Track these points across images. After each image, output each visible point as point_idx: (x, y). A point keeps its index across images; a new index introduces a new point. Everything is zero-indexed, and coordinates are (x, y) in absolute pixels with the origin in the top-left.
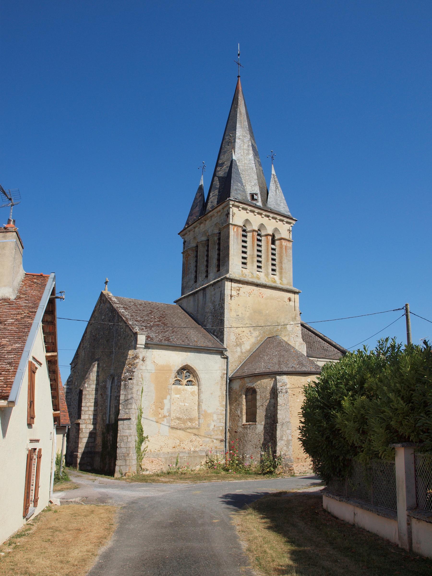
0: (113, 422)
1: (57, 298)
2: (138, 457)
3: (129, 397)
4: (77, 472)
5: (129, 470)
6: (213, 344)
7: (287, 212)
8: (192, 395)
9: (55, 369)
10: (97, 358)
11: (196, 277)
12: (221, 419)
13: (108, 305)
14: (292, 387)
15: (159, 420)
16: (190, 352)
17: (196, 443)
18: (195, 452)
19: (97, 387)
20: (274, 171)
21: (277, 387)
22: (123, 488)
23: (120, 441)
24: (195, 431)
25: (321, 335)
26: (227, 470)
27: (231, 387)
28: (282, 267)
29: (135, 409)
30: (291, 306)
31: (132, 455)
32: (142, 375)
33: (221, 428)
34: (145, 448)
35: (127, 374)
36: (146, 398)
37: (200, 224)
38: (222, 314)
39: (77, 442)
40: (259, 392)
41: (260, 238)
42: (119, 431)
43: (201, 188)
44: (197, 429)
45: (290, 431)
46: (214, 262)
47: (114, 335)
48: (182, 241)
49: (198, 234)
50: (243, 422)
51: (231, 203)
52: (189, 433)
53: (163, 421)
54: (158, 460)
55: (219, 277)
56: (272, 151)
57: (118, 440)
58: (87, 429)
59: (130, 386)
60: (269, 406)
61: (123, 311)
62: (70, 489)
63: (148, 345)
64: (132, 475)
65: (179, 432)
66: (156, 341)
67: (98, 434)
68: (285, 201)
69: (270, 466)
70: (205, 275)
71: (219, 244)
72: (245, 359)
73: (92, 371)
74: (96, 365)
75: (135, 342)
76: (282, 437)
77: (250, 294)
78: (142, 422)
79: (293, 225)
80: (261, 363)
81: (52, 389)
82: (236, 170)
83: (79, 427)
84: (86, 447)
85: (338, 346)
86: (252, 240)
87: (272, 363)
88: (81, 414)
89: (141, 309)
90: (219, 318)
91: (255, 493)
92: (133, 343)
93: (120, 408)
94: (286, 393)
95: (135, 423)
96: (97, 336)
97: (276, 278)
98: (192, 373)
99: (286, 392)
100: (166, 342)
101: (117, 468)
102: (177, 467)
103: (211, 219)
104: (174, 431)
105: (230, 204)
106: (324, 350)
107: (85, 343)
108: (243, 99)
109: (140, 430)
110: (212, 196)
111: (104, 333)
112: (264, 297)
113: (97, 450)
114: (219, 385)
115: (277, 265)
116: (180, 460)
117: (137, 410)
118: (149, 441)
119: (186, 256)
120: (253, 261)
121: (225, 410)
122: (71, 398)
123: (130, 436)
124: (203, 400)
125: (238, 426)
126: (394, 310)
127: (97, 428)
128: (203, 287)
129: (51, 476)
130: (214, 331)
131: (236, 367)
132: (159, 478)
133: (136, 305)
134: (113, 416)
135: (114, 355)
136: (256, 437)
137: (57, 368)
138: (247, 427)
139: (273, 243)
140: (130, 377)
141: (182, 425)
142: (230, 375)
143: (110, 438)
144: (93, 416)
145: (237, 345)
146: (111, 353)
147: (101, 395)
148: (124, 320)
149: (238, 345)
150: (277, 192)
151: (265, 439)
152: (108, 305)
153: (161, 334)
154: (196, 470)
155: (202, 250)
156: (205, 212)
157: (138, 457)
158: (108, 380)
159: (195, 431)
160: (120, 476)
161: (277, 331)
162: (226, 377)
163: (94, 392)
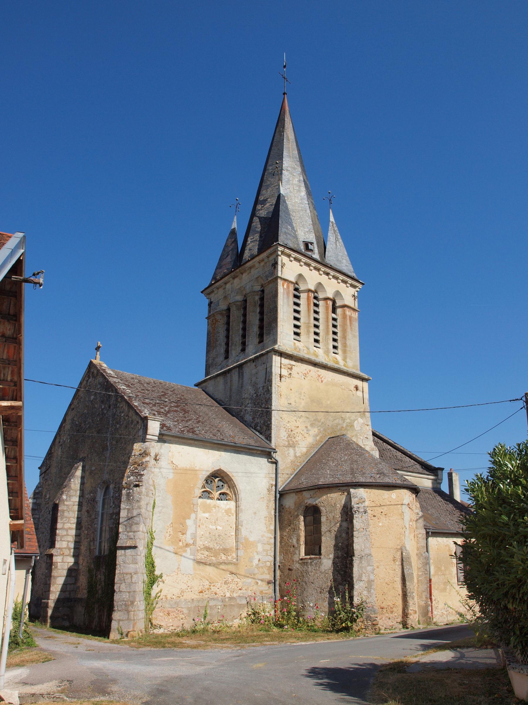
1: (26, 281)
2: (147, 607)
3: (135, 513)
4: (47, 630)
5: (134, 627)
6: (256, 442)
7: (351, 272)
8: (228, 515)
9: (17, 437)
10: (81, 457)
11: (227, 352)
12: (268, 550)
13: (101, 380)
14: (371, 505)
15: (179, 550)
16: (226, 451)
17: (233, 586)
18: (231, 598)
19: (81, 501)
20: (333, 217)
21: (351, 504)
22: (127, 657)
24: (231, 568)
25: (390, 441)
26: (281, 626)
27: (282, 505)
28: (345, 343)
30: (358, 397)
31: (139, 604)
32: (153, 481)
33: (268, 564)
34: (158, 593)
35: (132, 478)
36: (159, 517)
37: (234, 278)
38: (269, 400)
40: (325, 511)
41: (318, 303)
42: (118, 567)
43: (233, 233)
44: (234, 564)
45: (372, 567)
46: (254, 329)
47: (109, 423)
48: (207, 301)
49: (230, 292)
50: (301, 555)
51: (280, 249)
52: (223, 570)
53: (186, 551)
54: (177, 611)
55: (262, 350)
56: (330, 191)
57: (116, 580)
59: (136, 497)
60: (339, 531)
61: (123, 387)
62: (37, 661)
63: (164, 437)
64: (139, 635)
65: (210, 570)
66: (175, 431)
68: (348, 258)
69: (346, 620)
70: (240, 348)
71: (262, 306)
72: (301, 465)
73: (73, 476)
74: (80, 468)
75: (143, 431)
76: (360, 576)
77: (305, 375)
78: (153, 553)
79: (359, 290)
80: (326, 471)
81: (9, 476)
82: (285, 208)
83: (52, 560)
84: (63, 591)
85: (414, 456)
86: (307, 303)
87: (342, 471)
89: (149, 389)
91: (353, 664)
92: (141, 433)
93: (120, 530)
94: (365, 513)
95: (143, 554)
96: (83, 425)
97: (339, 357)
98: (227, 483)
99: (365, 512)
100: (190, 435)
101: (114, 625)
102: (206, 622)
103: (250, 271)
104: (202, 567)
106: (399, 460)
107: (63, 436)
108: (291, 122)
109: (151, 565)
110: (251, 242)
111: (92, 421)
112: (325, 381)
113: (79, 596)
114: (265, 501)
115: (339, 341)
117: (146, 534)
118: (164, 582)
119: (213, 321)
120: (309, 331)
121: (273, 537)
122: (39, 518)
123: (135, 574)
124: (242, 522)
125: (293, 561)
126: (510, 401)
127: (81, 562)
128: (238, 363)
129: (7, 583)
130: (256, 425)
132: (180, 640)
133: (142, 383)
135: (109, 452)
137: (21, 434)
139: (334, 311)
140: (137, 483)
141: (213, 558)
142: (280, 487)
143: (101, 576)
144: (75, 544)
145: (289, 446)
146: (105, 448)
147: (88, 511)
148: (126, 399)
149: (292, 445)
150: (338, 244)
151: (335, 580)
152: (101, 380)
153: (182, 423)
154: (234, 626)
155: (236, 315)
156: (240, 263)
157: (147, 607)
158: (99, 489)
159: (231, 568)
160: (119, 637)
161: (341, 430)
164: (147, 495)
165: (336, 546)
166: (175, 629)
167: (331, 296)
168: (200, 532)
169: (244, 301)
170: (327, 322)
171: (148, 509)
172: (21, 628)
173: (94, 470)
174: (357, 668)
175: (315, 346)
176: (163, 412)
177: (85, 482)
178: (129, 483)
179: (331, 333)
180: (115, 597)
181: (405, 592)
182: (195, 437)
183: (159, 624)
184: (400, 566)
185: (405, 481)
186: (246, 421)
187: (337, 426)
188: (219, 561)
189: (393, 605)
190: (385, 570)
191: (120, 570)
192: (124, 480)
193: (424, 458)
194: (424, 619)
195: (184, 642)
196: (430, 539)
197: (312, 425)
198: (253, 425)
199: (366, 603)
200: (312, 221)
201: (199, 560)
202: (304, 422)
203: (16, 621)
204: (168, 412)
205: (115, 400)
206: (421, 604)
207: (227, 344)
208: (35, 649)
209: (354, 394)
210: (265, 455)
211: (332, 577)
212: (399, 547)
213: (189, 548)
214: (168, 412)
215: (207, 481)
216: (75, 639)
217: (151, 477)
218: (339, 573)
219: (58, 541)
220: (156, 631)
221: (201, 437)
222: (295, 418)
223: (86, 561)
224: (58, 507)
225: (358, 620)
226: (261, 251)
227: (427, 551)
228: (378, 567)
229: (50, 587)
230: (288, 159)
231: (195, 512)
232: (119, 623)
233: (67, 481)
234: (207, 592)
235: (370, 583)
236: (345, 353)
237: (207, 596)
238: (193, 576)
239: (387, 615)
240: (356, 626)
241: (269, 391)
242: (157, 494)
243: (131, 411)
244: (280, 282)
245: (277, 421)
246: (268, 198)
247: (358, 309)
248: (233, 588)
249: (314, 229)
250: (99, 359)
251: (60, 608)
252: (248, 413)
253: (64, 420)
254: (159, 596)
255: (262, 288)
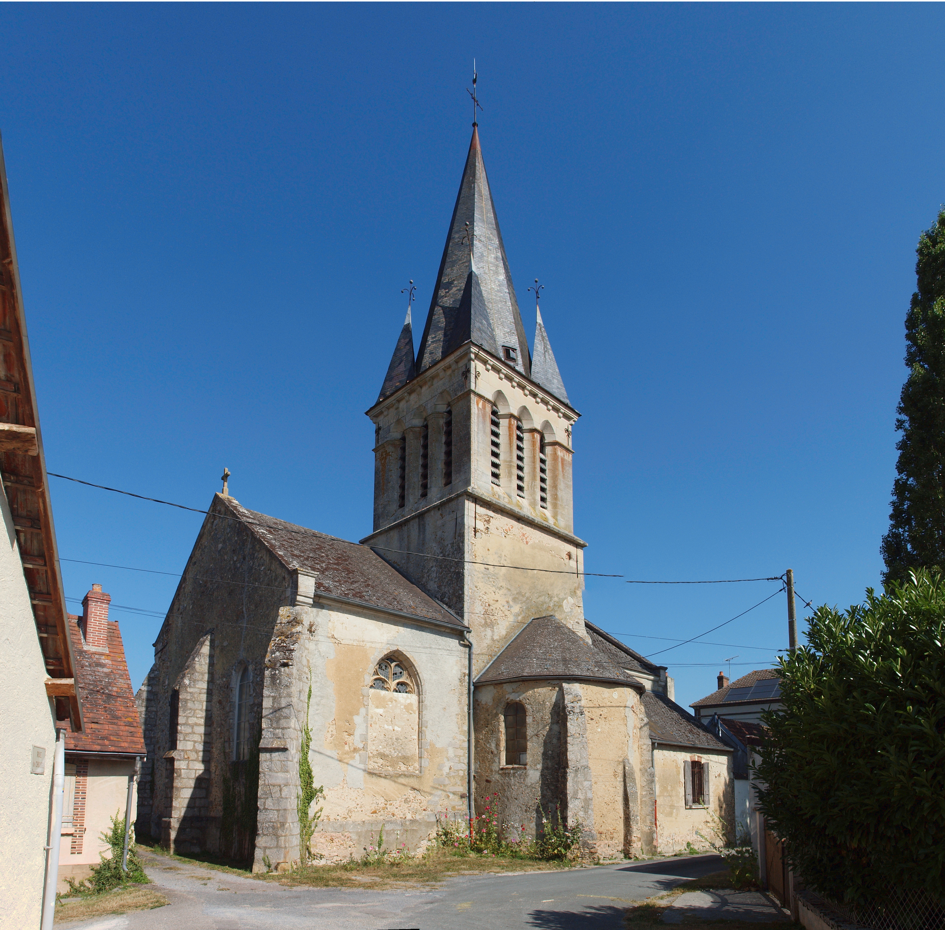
0: (245, 759)
2: (302, 831)
5: (285, 857)
6: (444, 617)
10: (208, 629)
11: (402, 497)
13: (230, 520)
14: (588, 706)
16: (404, 625)
17: (415, 805)
18: (413, 821)
19: (210, 688)
20: (540, 318)
21: (564, 702)
23: (264, 796)
24: (413, 782)
27: (477, 701)
28: (556, 495)
29: (296, 730)
31: (292, 826)
32: (308, 661)
34: (317, 813)
35: (277, 654)
36: (317, 710)
37: (410, 394)
38: (460, 563)
39: (170, 796)
40: (531, 710)
41: (521, 435)
42: (261, 775)
43: (407, 330)
45: (589, 783)
48: (374, 427)
49: (405, 413)
50: (501, 764)
51: (474, 349)
53: (353, 758)
54: (343, 837)
55: (450, 494)
56: (537, 279)
57: (259, 794)
58: (191, 771)
59: (285, 680)
61: (263, 531)
63: (321, 601)
64: (292, 867)
67: (214, 781)
68: (560, 377)
70: (420, 492)
71: (449, 433)
72: (499, 650)
73: (198, 653)
74: (208, 643)
76: (576, 793)
77: (506, 532)
78: (309, 759)
79: (573, 423)
82: (478, 293)
83: (173, 765)
84: (190, 806)
86: (508, 434)
88: (177, 740)
90: (452, 570)
92: (288, 593)
93: (264, 726)
94: (581, 715)
95: (296, 760)
98: (406, 669)
99: (582, 713)
101: (258, 853)
102: (382, 850)
103: (432, 382)
104: (374, 779)
105: (471, 352)
106: (614, 654)
113: (212, 814)
115: (547, 491)
116: (387, 837)
117: (299, 733)
118: (325, 798)
119: (382, 455)
120: (511, 472)
121: (466, 740)
123: (285, 785)
124: (427, 722)
127: (213, 769)
130: (443, 595)
131: (483, 664)
134: (246, 747)
136: (527, 791)
138: (509, 774)
140: (285, 661)
142: (475, 677)
143: (241, 789)
144: (204, 746)
145: (486, 625)
147: (220, 702)
148: (267, 546)
149: (489, 624)
150: (547, 357)
151: (543, 796)
157: (302, 831)
158: (234, 672)
159: (413, 782)
160: (265, 870)
161: (548, 610)
162: (467, 681)
163: (205, 696)
164: (300, 679)
165: (544, 754)
166: (341, 860)
167: (539, 428)
168: (372, 734)
169: (424, 426)
170: (534, 463)
171: (302, 698)
172: (125, 858)
173: (227, 646)
174: (595, 914)
175: (518, 495)
176: (318, 569)
177: (215, 662)
178: (274, 661)
179: (539, 479)
180: (258, 816)
181: (628, 815)
182: (364, 603)
183: (320, 853)
184: (622, 783)
185: (629, 677)
186: (429, 590)
187: (542, 605)
188: (398, 772)
189: (614, 829)
190: (604, 786)
191: (264, 781)
192: (267, 656)
193: (642, 653)
194: (647, 848)
195: (354, 878)
196: (656, 752)
197: (514, 600)
198: (439, 595)
199: (583, 827)
200: (514, 318)
201: (372, 771)
202: (505, 595)
203: (116, 847)
204: (326, 569)
205: (252, 548)
206: (645, 830)
207: (402, 487)
208: (145, 887)
209: (567, 564)
210: (456, 635)
211: (540, 793)
212: (621, 759)
213: (358, 754)
214: (326, 569)
215: (380, 664)
216: (206, 871)
217: (304, 655)
218: (549, 787)
219: (180, 741)
220: (316, 863)
221: (372, 604)
222: (494, 589)
223: (219, 768)
224: (178, 695)
225: (573, 847)
226: (445, 354)
227: (652, 766)
228: (596, 783)
229: (172, 801)
230: (480, 224)
231: (366, 706)
232: (265, 852)
233: (189, 660)
234: (382, 812)
235: (587, 802)
236: (556, 508)
237: (382, 818)
238: (363, 790)
239: (606, 842)
240: (571, 853)
241: (459, 550)
242: (313, 679)
243: (274, 562)
244: (474, 399)
245: (470, 591)
246: (454, 280)
247: (573, 449)
248: (415, 807)
249: (517, 330)
250: (227, 493)
251: (187, 830)
252: (432, 580)
253: (184, 579)
254: (319, 817)
255: (449, 408)
